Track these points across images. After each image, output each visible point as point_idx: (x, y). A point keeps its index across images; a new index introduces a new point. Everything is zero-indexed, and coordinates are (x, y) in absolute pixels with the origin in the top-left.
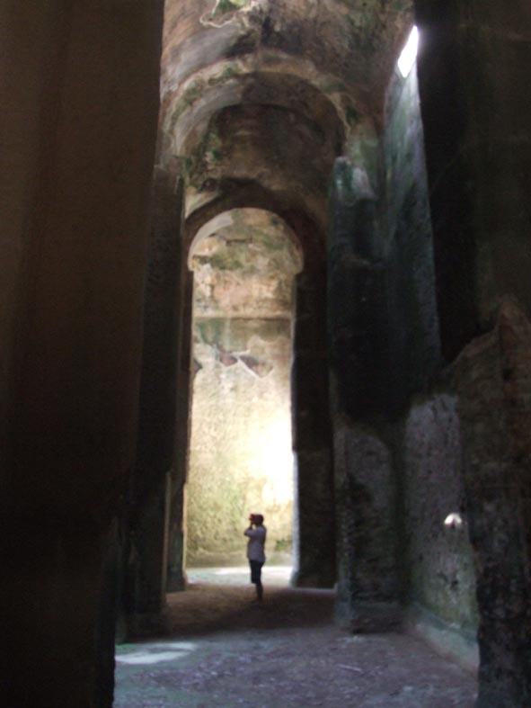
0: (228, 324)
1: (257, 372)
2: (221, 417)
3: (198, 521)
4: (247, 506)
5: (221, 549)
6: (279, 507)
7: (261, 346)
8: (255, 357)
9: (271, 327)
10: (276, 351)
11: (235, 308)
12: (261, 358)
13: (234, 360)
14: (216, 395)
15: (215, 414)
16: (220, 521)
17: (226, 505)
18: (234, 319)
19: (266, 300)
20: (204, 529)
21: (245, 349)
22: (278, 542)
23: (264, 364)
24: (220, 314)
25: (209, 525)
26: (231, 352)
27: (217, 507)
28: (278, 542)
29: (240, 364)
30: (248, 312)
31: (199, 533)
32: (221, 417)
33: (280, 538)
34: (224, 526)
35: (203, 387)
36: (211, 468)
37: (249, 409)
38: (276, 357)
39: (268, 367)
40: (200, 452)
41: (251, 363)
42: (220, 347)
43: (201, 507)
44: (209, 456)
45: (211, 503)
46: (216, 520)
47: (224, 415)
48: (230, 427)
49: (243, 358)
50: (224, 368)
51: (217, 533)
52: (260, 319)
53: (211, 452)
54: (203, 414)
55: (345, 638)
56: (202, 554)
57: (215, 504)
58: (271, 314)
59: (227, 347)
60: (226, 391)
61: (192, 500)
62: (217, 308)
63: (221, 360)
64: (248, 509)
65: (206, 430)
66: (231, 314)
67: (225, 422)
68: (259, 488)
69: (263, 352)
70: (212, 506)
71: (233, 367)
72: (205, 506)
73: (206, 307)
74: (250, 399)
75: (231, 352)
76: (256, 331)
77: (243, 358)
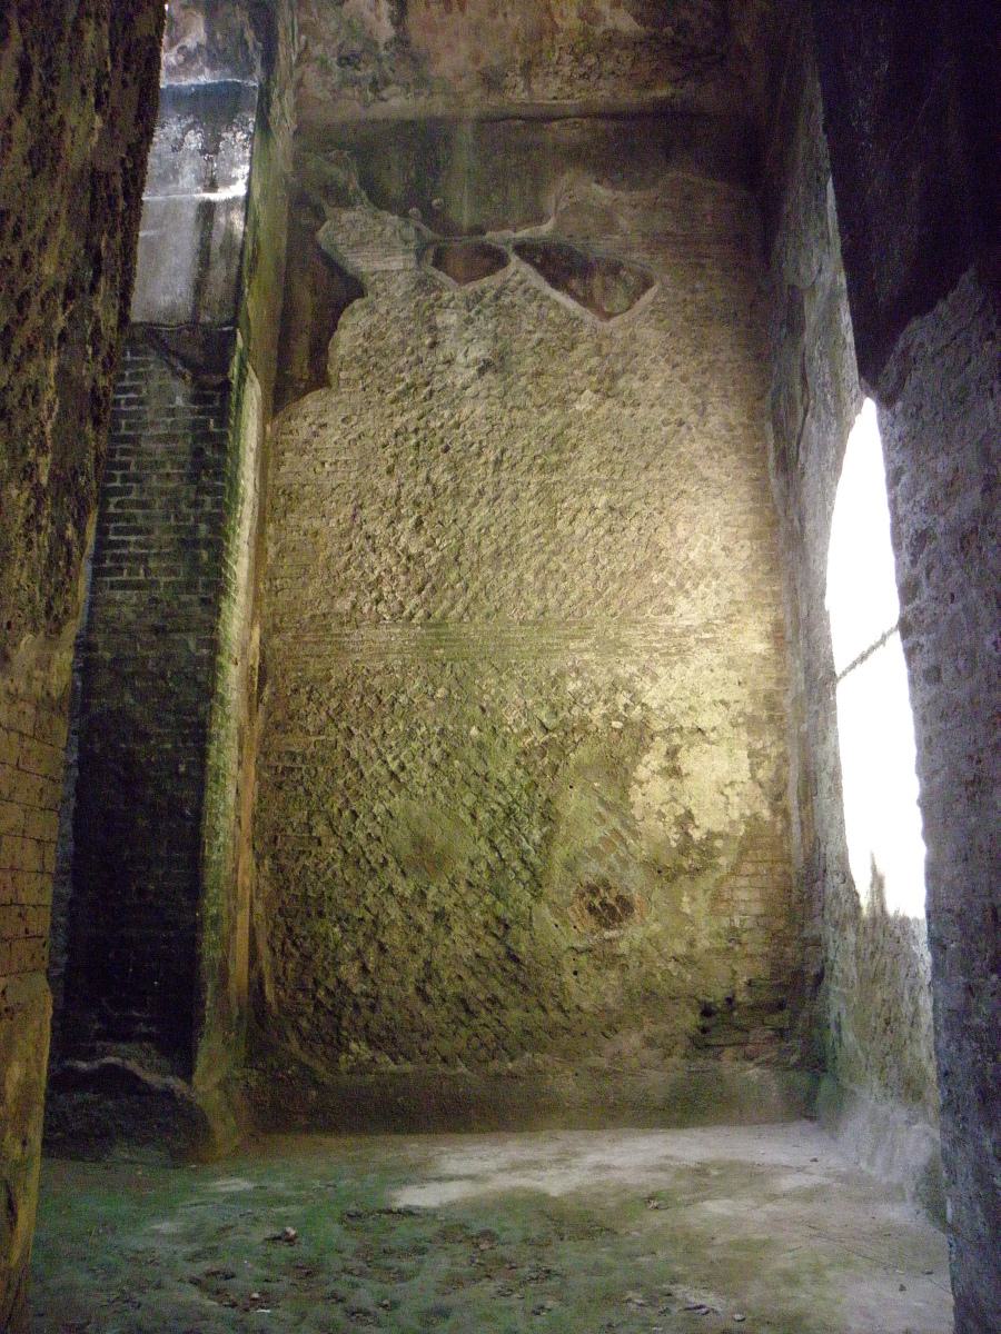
0: (465, 135)
1: (586, 301)
2: (442, 477)
3: (342, 920)
4: (560, 853)
5: (446, 1046)
6: (707, 850)
7: (582, 202)
8: (578, 245)
9: (625, 143)
10: (661, 222)
11: (491, 81)
12: (602, 247)
13: (494, 260)
14: (423, 389)
15: (416, 464)
16: (440, 916)
17: (470, 851)
18: (486, 121)
19: (613, 39)
20: (372, 958)
21: (539, 218)
22: (707, 1012)
23: (615, 269)
24: (439, 106)
25: (393, 938)
26: (479, 230)
27: (427, 858)
28: (707, 1012)
29: (517, 269)
30: (548, 91)
31: (349, 971)
32: (442, 477)
33: (718, 994)
34: (461, 942)
35: (367, 361)
36: (399, 689)
37: (557, 442)
38: (656, 242)
39: (889, 428)
40: (353, 618)
41: (559, 265)
42: (432, 216)
43: (354, 860)
44: (392, 636)
45: (401, 837)
46: (423, 918)
47: (455, 466)
48: (482, 514)
49: (523, 250)
50: (453, 292)
51: (430, 973)
52: (586, 114)
53: (401, 616)
54: (365, 468)
55: (829, 891)
56: (360, 1069)
57: (420, 843)
58: (630, 98)
59: (464, 214)
60: (462, 374)
61: (321, 829)
62: (422, 82)
63: (439, 262)
64: (569, 867)
65: (378, 529)
66: (476, 102)
67: (458, 494)
68: (617, 771)
69: (609, 226)
70: (407, 850)
71: (490, 283)
72: (376, 854)
73: (377, 85)
74: (563, 402)
75: (479, 230)
76: (577, 156)
77: (523, 250)
